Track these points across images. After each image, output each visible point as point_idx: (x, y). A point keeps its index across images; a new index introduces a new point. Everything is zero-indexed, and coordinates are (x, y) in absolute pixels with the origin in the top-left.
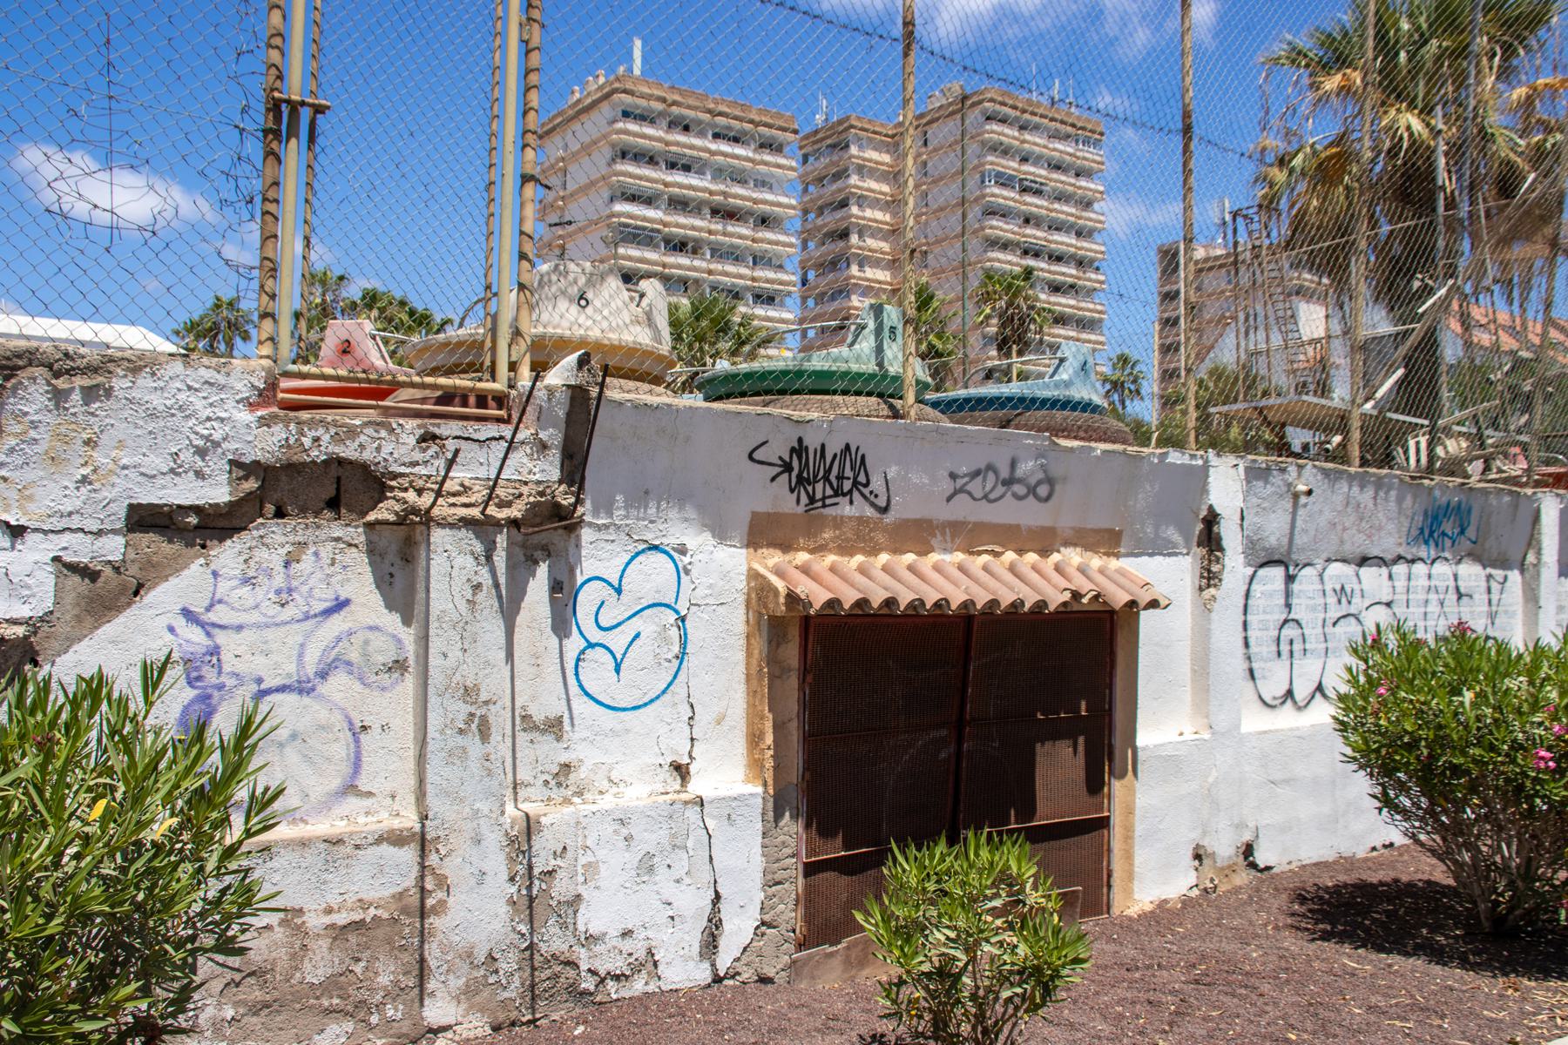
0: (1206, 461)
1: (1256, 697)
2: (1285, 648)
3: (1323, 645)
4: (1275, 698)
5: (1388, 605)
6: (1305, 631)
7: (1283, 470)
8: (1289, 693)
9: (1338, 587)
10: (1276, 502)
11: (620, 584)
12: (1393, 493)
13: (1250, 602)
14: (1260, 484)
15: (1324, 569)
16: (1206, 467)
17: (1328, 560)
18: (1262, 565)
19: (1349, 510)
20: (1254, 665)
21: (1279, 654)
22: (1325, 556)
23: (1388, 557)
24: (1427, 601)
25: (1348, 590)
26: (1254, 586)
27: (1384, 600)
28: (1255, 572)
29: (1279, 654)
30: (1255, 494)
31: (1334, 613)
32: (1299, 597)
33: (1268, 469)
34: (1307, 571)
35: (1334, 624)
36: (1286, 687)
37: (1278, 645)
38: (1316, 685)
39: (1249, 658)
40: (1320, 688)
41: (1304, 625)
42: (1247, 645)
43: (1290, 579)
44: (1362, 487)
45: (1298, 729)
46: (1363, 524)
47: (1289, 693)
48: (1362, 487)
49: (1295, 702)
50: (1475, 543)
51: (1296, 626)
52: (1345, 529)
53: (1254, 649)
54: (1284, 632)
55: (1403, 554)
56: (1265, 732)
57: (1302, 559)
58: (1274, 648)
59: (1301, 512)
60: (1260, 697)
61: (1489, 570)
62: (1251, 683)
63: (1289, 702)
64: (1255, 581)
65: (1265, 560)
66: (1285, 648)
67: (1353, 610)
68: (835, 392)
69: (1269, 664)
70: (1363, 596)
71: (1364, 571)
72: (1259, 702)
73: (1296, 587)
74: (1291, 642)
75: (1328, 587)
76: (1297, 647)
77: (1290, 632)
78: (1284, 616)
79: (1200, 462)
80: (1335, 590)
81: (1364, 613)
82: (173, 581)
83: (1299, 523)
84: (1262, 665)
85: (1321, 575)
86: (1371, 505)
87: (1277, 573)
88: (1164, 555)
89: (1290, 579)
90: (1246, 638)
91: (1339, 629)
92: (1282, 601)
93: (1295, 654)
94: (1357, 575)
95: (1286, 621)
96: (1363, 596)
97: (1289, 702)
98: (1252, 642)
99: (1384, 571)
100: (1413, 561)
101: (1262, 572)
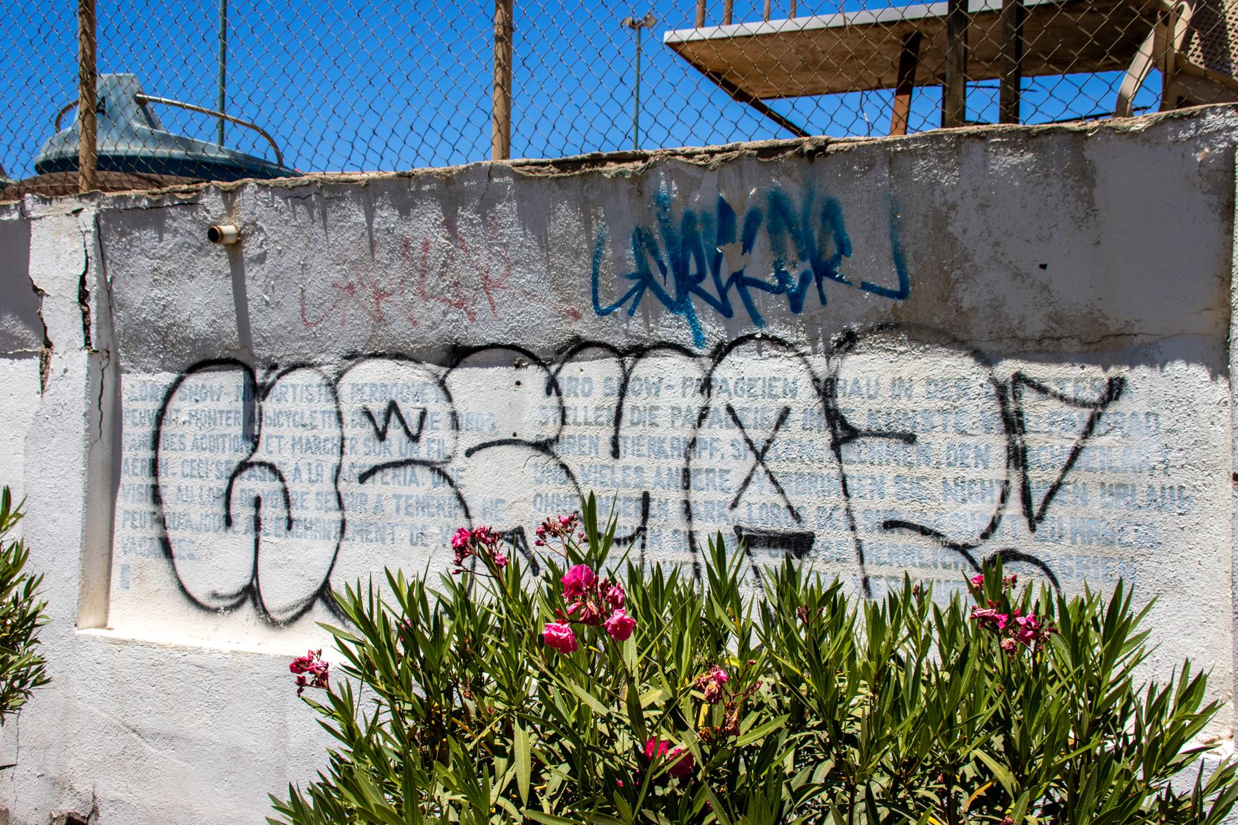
0: (23, 213)
1: (174, 587)
2: (242, 513)
3: (337, 516)
4: (215, 595)
5: (544, 446)
6: (289, 484)
7: (191, 205)
8: (251, 593)
9: (378, 408)
10: (190, 261)
11: (805, 362)
12: (506, 211)
13: (165, 429)
14: (150, 233)
15: (340, 375)
16: (26, 220)
17: (353, 356)
18: (193, 369)
19: (382, 255)
20: (172, 535)
21: (228, 521)
22: (343, 347)
23: (537, 343)
24: (693, 443)
25: (411, 413)
26: (175, 403)
27: (529, 435)
28: (179, 381)
29: (228, 521)
30: (143, 252)
31: (364, 453)
32: (275, 424)
33: (156, 206)
34: (300, 377)
35: (363, 478)
36: (244, 579)
37: (227, 505)
38: (315, 588)
39: (162, 521)
40: (324, 593)
41: (285, 475)
42: (157, 498)
43: (255, 392)
44: (405, 210)
45: (198, 651)
46: (431, 280)
47: (251, 593)
48: (405, 210)
49: (262, 609)
50: (902, 294)
51: (269, 474)
52: (380, 295)
53: (171, 505)
54: (239, 484)
55: (586, 334)
56: (125, 642)
57: (283, 354)
58: (220, 509)
59: (251, 271)
60: (182, 588)
61: (1006, 369)
62: (163, 563)
63: (248, 606)
64: (177, 395)
65: (195, 359)
66: (242, 513)
67: (423, 451)
68: (944, 107)
69: (203, 537)
70: (456, 426)
71: (458, 378)
72: (180, 597)
73: (269, 406)
74: (257, 502)
75: (350, 407)
76: (272, 512)
77: (248, 485)
78: (242, 456)
79: (16, 216)
80: (368, 414)
81: (460, 461)
82: (84, 372)
83: (254, 291)
84: (187, 534)
85: (332, 387)
86: (440, 238)
87: (233, 380)
88: (12, 357)
89: (255, 392)
90: (155, 488)
91: (374, 487)
92: (238, 430)
93: (265, 525)
94: (442, 383)
95: (244, 466)
96: (456, 426)
97: (248, 606)
98: (167, 494)
99: (534, 377)
100: (639, 352)
101: (192, 381)
